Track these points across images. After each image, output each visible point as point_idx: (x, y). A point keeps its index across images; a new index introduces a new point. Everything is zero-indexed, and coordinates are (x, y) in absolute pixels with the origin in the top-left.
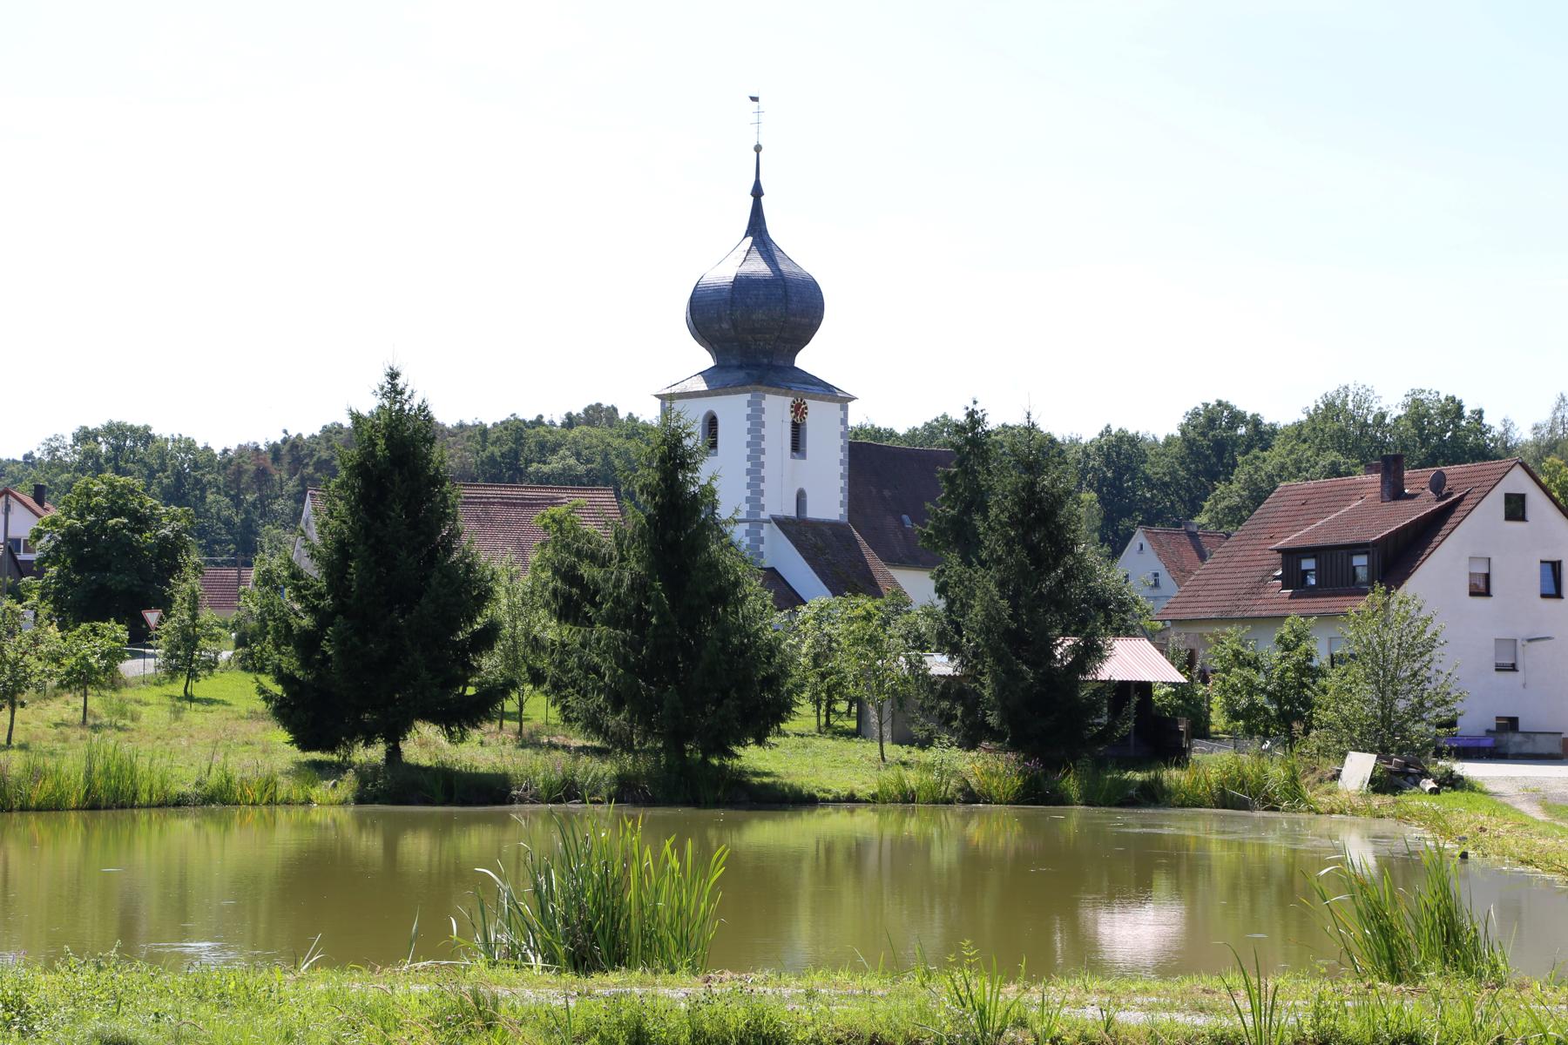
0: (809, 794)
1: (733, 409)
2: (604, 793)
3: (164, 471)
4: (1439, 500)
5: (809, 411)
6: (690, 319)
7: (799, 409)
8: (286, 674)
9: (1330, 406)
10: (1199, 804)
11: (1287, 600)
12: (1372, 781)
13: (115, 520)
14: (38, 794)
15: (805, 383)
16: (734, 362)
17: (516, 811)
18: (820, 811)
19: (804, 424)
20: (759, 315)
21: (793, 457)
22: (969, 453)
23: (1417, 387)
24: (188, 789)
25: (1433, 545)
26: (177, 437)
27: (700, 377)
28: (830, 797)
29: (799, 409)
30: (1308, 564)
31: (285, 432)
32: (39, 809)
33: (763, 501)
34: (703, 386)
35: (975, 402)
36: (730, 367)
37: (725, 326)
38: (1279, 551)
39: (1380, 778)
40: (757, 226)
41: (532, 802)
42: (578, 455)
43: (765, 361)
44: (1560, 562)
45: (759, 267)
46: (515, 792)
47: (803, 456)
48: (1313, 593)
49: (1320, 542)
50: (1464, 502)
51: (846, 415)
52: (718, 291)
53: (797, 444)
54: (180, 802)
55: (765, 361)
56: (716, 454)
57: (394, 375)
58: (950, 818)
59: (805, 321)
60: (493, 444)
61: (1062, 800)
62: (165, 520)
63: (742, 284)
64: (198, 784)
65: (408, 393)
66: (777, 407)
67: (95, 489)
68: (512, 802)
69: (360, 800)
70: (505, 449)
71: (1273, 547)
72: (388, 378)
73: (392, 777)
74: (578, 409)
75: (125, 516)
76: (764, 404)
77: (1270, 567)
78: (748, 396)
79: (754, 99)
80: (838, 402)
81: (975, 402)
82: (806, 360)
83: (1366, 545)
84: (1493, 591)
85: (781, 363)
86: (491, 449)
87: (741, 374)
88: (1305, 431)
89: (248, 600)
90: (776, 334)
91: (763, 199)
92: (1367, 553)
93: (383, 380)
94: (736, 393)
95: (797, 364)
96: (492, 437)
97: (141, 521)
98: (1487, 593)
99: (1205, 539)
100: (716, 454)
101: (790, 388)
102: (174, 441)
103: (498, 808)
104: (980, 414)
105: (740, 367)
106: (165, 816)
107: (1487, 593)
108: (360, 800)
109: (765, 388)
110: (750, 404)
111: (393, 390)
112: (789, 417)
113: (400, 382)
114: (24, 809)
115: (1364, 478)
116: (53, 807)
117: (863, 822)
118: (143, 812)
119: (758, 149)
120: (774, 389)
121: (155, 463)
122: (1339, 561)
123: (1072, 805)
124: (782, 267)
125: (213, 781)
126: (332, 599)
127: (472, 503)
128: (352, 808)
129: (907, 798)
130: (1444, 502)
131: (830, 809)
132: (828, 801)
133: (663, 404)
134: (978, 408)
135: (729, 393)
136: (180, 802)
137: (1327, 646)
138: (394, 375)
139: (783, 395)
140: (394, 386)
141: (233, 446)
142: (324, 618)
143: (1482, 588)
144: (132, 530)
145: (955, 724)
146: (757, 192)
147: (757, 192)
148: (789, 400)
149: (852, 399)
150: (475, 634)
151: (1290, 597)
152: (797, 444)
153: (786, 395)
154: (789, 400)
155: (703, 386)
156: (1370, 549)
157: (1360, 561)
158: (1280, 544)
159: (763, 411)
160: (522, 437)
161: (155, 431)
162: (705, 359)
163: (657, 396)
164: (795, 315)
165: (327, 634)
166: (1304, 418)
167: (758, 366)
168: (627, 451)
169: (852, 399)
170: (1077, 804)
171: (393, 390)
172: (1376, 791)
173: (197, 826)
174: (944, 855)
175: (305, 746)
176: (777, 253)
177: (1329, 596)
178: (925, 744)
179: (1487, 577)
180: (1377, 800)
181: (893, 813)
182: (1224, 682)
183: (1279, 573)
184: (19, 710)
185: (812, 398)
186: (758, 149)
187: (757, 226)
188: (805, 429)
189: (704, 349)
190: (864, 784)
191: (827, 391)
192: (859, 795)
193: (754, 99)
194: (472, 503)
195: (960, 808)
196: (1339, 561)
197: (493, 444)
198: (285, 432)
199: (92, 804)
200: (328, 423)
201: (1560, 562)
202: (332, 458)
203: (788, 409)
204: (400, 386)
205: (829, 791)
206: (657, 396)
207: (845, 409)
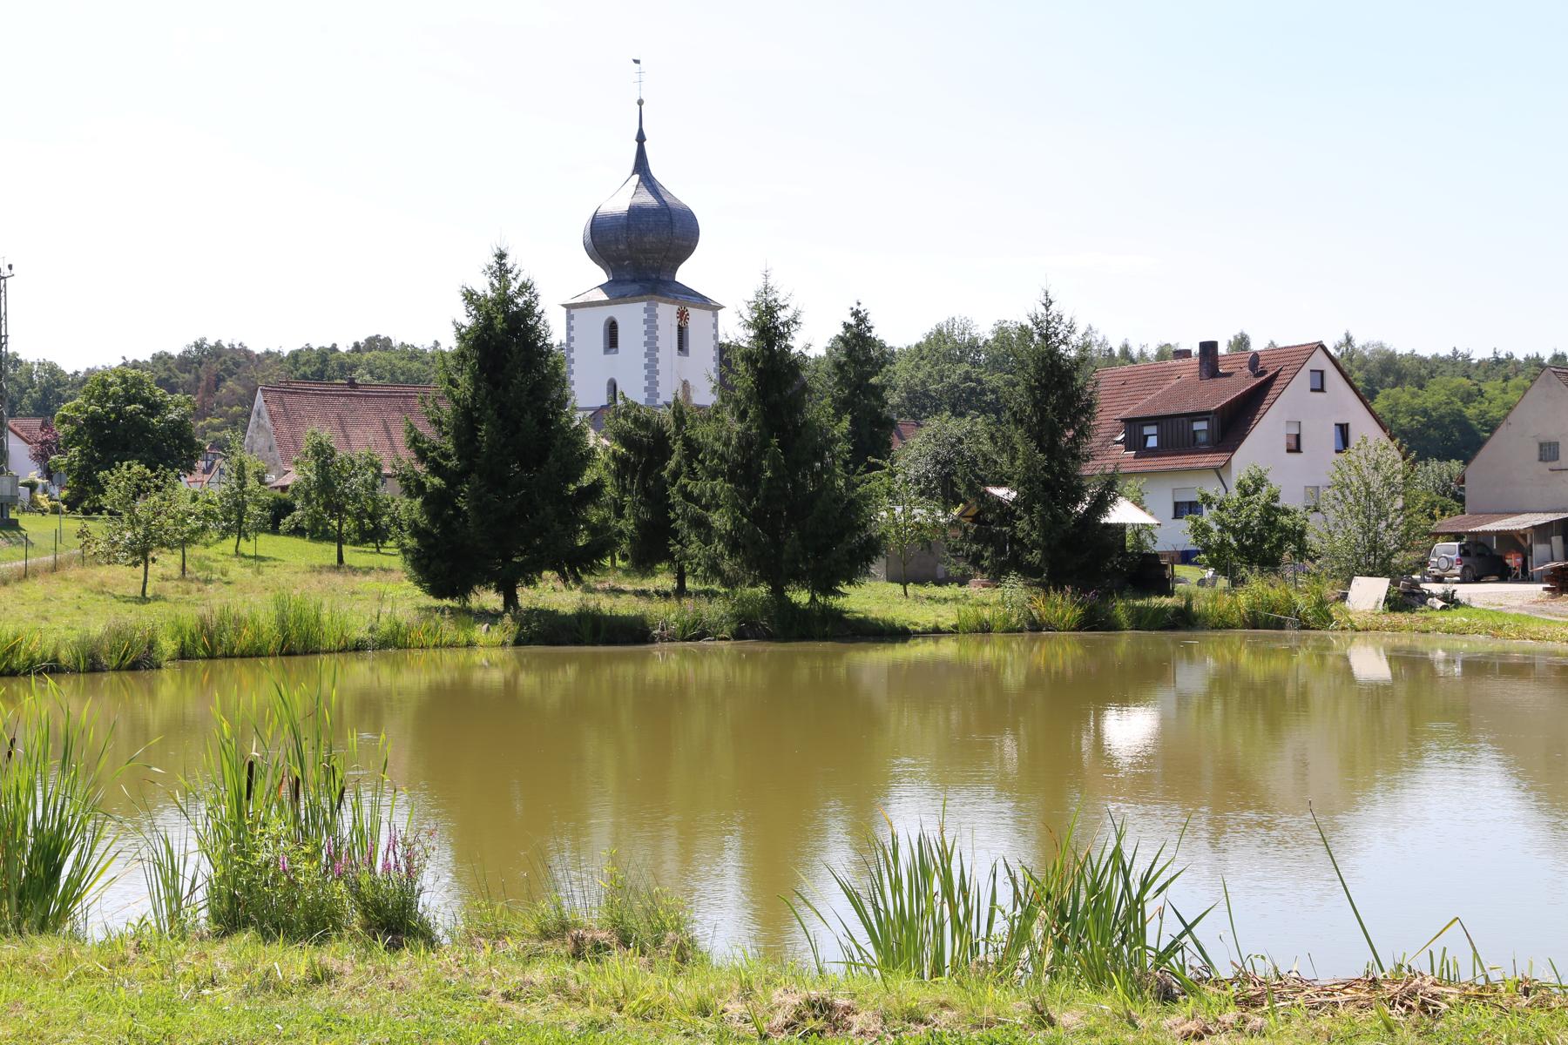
0: (902, 627)
1: (631, 316)
2: (726, 632)
3: (33, 388)
4: (1257, 376)
5: (690, 317)
6: (589, 239)
7: (682, 315)
8: (423, 528)
9: (940, 332)
10: (1230, 627)
11: (1133, 460)
12: (1387, 600)
13: (133, 406)
14: (242, 644)
15: (686, 294)
16: (628, 277)
17: (657, 649)
18: (911, 642)
19: (687, 327)
20: (650, 238)
21: (679, 354)
22: (855, 345)
23: (1002, 319)
24: (359, 632)
25: (1261, 412)
26: (42, 361)
27: (599, 289)
28: (919, 629)
29: (682, 315)
30: (1149, 430)
31: (124, 358)
32: (242, 656)
33: (658, 390)
34: (604, 297)
35: (859, 304)
36: (625, 280)
37: (621, 247)
38: (1122, 420)
39: (1395, 599)
40: (641, 165)
41: (669, 641)
42: (371, 373)
43: (654, 276)
44: (1347, 425)
45: (647, 199)
46: (656, 632)
47: (687, 354)
48: (1154, 453)
49: (1162, 412)
50: (1279, 378)
51: (717, 320)
52: (615, 218)
53: (682, 345)
54: (358, 648)
55: (654, 276)
56: (617, 352)
57: (501, 256)
58: (1017, 644)
59: (686, 243)
60: (304, 364)
61: (1111, 626)
62: (171, 407)
63: (635, 212)
64: (372, 630)
65: (515, 271)
66: (667, 313)
67: (110, 380)
68: (653, 641)
69: (518, 642)
70: (314, 369)
71: (1117, 417)
72: (496, 258)
73: (546, 620)
74: (361, 340)
75: (140, 403)
76: (658, 311)
77: (1108, 434)
78: (644, 304)
79: (637, 62)
80: (711, 310)
81: (859, 304)
82: (686, 274)
83: (1209, 413)
84: (1302, 449)
85: (666, 278)
86: (303, 368)
87: (636, 287)
88: (925, 352)
89: (304, 468)
90: (664, 254)
91: (645, 143)
92: (1207, 419)
93: (492, 261)
94: (633, 302)
95: (676, 280)
96: (302, 359)
97: (154, 408)
98: (1297, 449)
99: (903, 427)
100: (617, 352)
101: (676, 298)
102: (39, 364)
103: (642, 648)
104: (863, 314)
105: (634, 281)
106: (346, 660)
107: (1297, 449)
108: (518, 642)
109: (658, 297)
110: (646, 310)
111: (501, 270)
112: (676, 322)
113: (509, 262)
114: (230, 655)
115: (1175, 362)
116: (254, 653)
117: (948, 648)
118: (326, 657)
119: (640, 103)
120: (665, 299)
121: (25, 383)
122: (1180, 426)
123: (1123, 630)
124: (666, 199)
125: (385, 627)
126: (458, 459)
127: (394, 397)
128: (509, 650)
129: (984, 629)
130: (1263, 378)
131: (920, 640)
132: (918, 633)
133: (568, 312)
134: (861, 309)
135: (627, 302)
136: (358, 648)
137: (1171, 496)
138: (501, 256)
139: (671, 303)
140: (501, 265)
141: (82, 370)
142: (453, 478)
143: (1295, 447)
144: (145, 415)
145: (986, 563)
146: (641, 138)
147: (641, 138)
148: (676, 308)
149: (721, 307)
150: (580, 490)
151: (1135, 457)
152: (682, 345)
153: (673, 303)
154: (676, 308)
155: (604, 297)
156: (1210, 417)
157: (1200, 426)
158: (1124, 414)
159: (656, 316)
160: (326, 360)
161: (21, 357)
162: (601, 276)
163: (563, 305)
164: (678, 239)
165: (463, 491)
166: (924, 340)
167: (649, 280)
168: (409, 370)
169: (721, 307)
170: (1126, 629)
171: (501, 270)
172: (1392, 609)
173: (372, 669)
174: (1013, 677)
175: (438, 592)
176: (660, 188)
177: (1173, 455)
178: (963, 581)
179: (1298, 437)
180: (1399, 618)
181: (971, 640)
182: (1195, 522)
183: (1120, 437)
184: (151, 566)
185: (693, 307)
186: (640, 103)
187: (641, 165)
188: (687, 332)
189: (599, 267)
190: (947, 616)
191: (703, 302)
192: (942, 626)
193: (637, 62)
194: (394, 397)
195: (1027, 635)
196: (1180, 426)
197: (304, 364)
198: (124, 358)
199: (287, 651)
200: (157, 351)
201: (1347, 425)
202: (170, 377)
203: (675, 315)
204: (509, 266)
205: (916, 624)
206: (563, 305)
207: (715, 315)
